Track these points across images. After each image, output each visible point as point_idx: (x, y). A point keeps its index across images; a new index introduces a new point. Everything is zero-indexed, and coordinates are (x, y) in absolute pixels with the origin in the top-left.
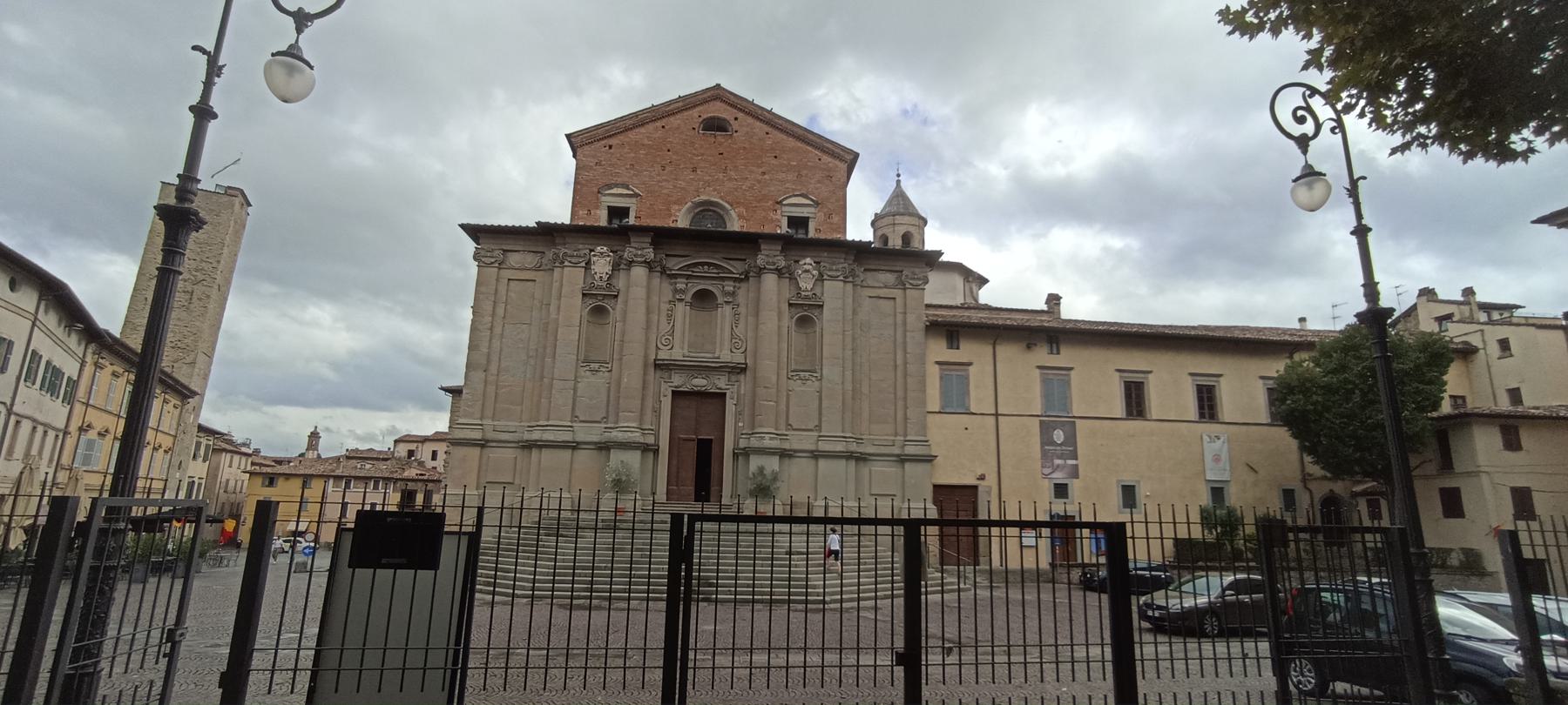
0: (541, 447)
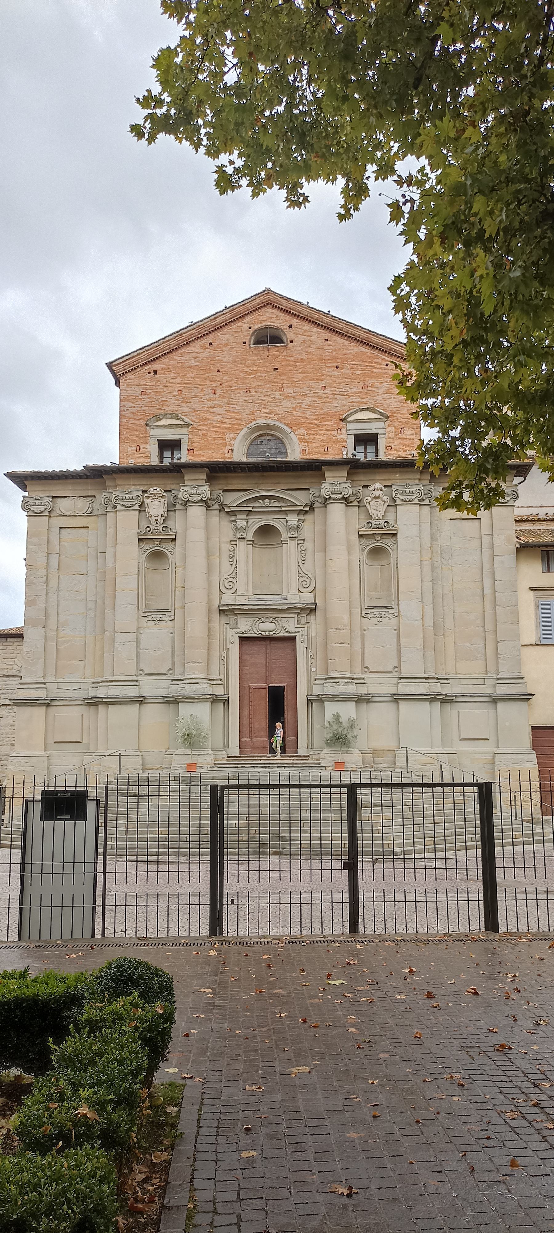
0: (107, 703)
